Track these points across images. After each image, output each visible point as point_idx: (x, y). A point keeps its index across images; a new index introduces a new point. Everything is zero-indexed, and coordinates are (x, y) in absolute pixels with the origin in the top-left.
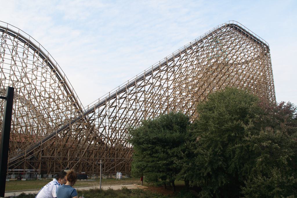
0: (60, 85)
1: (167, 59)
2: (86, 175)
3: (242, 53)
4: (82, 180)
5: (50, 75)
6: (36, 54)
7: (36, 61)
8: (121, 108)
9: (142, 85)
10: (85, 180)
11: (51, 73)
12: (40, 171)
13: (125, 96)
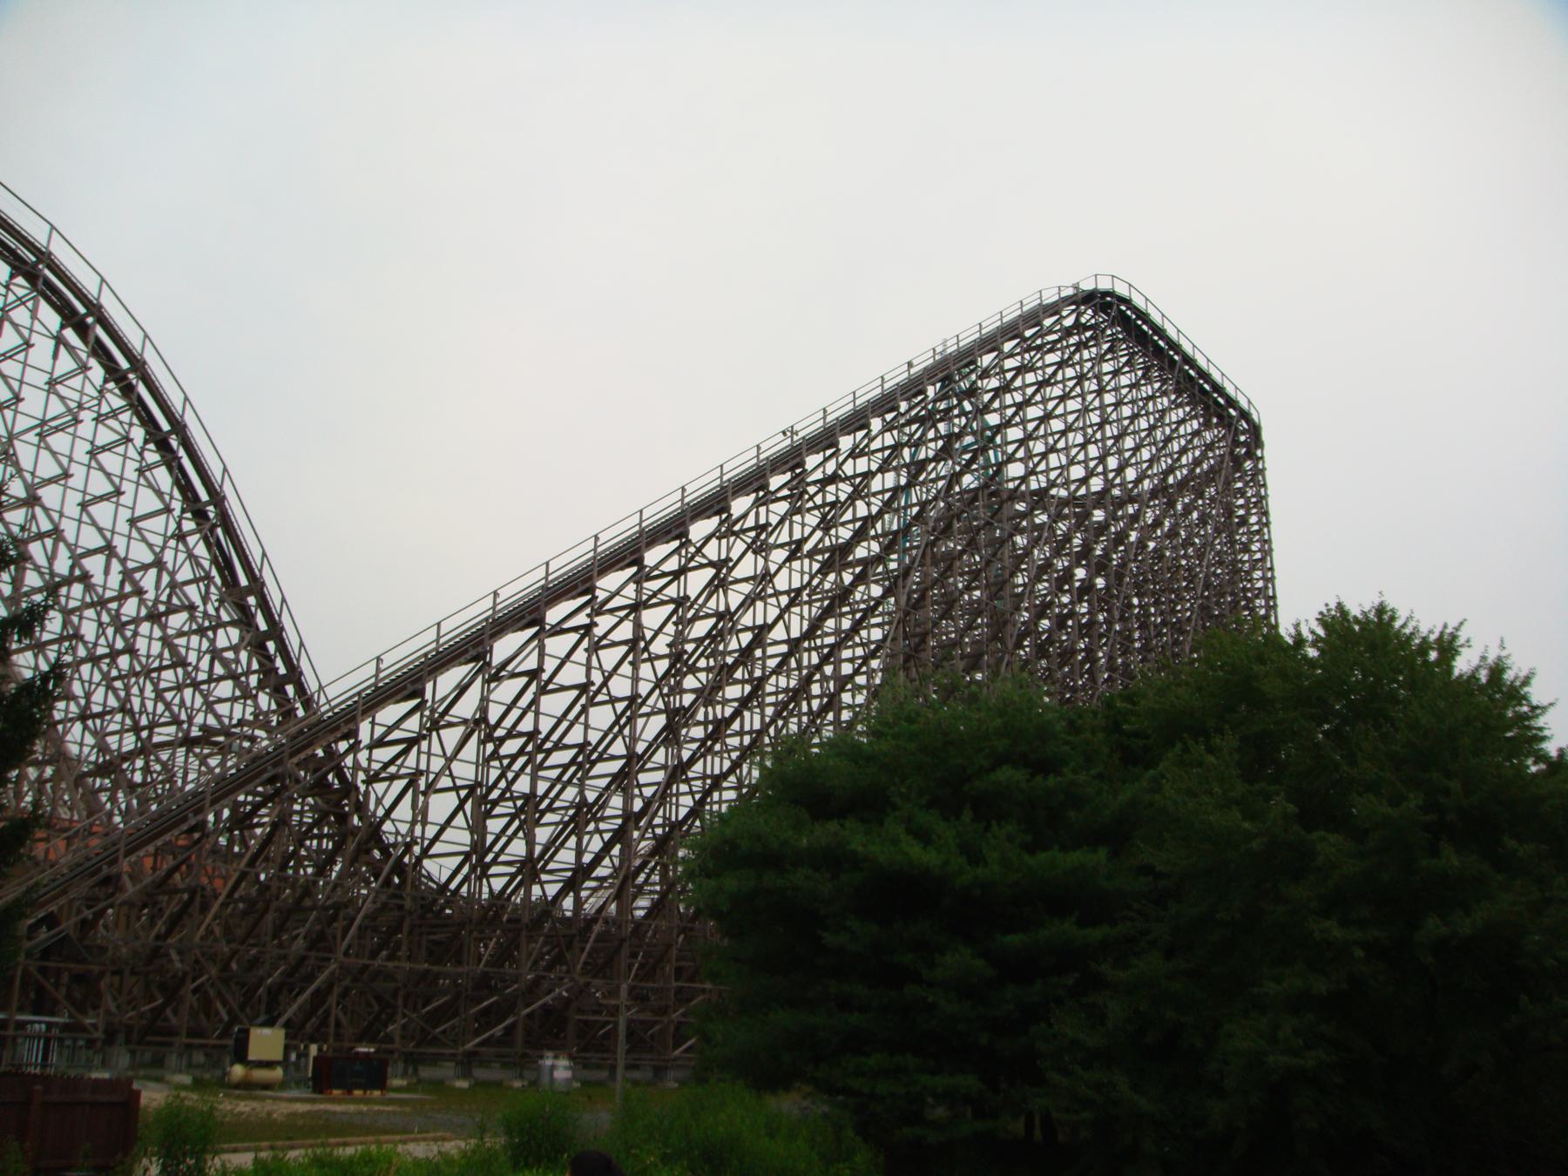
0: (189, 525)
1: (794, 433)
2: (383, 1065)
3: (1017, 425)
4: (358, 1093)
5: (137, 465)
6: (70, 335)
7: (70, 375)
8: (551, 687)
9: (668, 567)
10: (377, 1093)
11: (141, 454)
12: (101, 1027)
13: (582, 619)
